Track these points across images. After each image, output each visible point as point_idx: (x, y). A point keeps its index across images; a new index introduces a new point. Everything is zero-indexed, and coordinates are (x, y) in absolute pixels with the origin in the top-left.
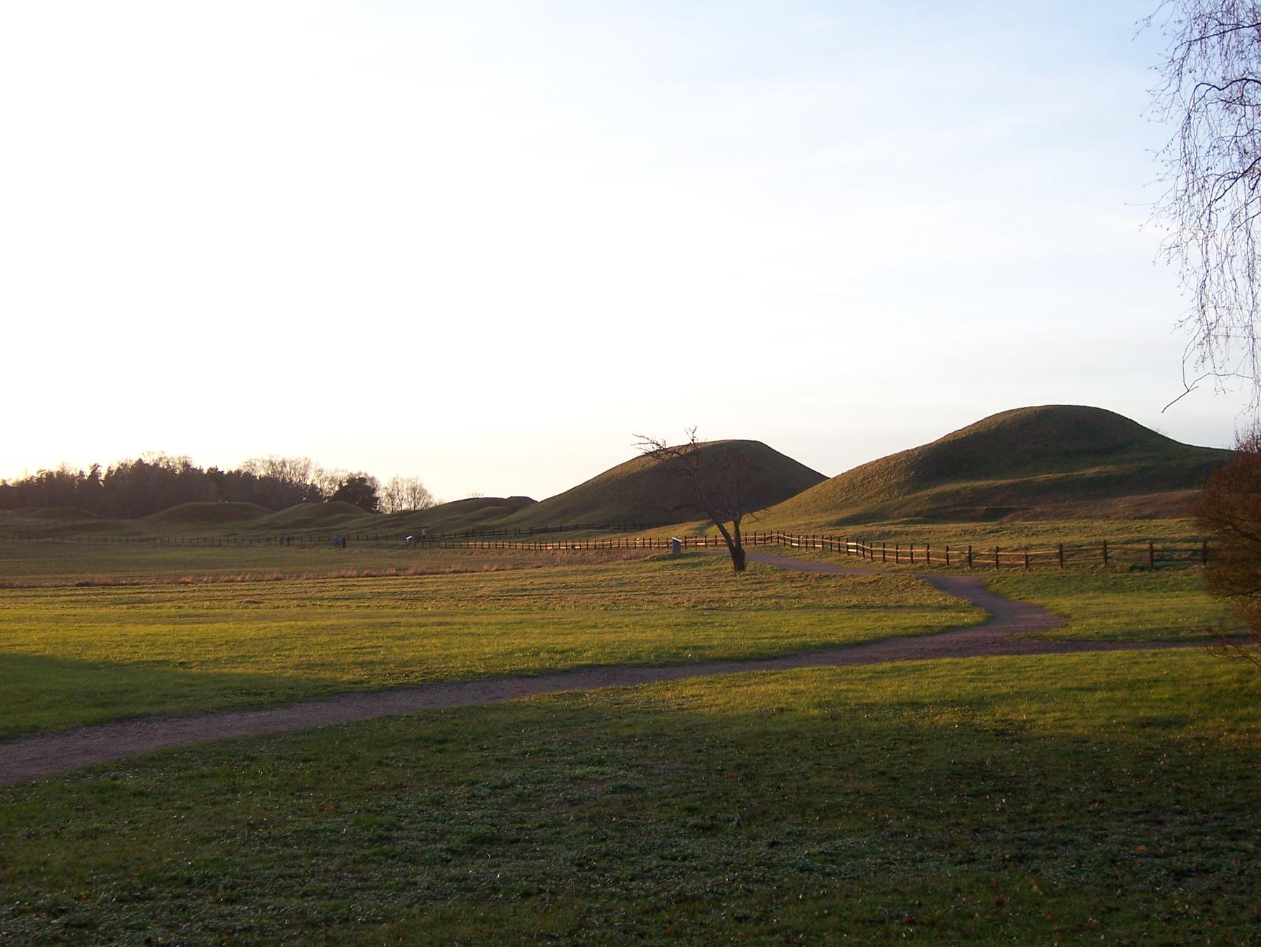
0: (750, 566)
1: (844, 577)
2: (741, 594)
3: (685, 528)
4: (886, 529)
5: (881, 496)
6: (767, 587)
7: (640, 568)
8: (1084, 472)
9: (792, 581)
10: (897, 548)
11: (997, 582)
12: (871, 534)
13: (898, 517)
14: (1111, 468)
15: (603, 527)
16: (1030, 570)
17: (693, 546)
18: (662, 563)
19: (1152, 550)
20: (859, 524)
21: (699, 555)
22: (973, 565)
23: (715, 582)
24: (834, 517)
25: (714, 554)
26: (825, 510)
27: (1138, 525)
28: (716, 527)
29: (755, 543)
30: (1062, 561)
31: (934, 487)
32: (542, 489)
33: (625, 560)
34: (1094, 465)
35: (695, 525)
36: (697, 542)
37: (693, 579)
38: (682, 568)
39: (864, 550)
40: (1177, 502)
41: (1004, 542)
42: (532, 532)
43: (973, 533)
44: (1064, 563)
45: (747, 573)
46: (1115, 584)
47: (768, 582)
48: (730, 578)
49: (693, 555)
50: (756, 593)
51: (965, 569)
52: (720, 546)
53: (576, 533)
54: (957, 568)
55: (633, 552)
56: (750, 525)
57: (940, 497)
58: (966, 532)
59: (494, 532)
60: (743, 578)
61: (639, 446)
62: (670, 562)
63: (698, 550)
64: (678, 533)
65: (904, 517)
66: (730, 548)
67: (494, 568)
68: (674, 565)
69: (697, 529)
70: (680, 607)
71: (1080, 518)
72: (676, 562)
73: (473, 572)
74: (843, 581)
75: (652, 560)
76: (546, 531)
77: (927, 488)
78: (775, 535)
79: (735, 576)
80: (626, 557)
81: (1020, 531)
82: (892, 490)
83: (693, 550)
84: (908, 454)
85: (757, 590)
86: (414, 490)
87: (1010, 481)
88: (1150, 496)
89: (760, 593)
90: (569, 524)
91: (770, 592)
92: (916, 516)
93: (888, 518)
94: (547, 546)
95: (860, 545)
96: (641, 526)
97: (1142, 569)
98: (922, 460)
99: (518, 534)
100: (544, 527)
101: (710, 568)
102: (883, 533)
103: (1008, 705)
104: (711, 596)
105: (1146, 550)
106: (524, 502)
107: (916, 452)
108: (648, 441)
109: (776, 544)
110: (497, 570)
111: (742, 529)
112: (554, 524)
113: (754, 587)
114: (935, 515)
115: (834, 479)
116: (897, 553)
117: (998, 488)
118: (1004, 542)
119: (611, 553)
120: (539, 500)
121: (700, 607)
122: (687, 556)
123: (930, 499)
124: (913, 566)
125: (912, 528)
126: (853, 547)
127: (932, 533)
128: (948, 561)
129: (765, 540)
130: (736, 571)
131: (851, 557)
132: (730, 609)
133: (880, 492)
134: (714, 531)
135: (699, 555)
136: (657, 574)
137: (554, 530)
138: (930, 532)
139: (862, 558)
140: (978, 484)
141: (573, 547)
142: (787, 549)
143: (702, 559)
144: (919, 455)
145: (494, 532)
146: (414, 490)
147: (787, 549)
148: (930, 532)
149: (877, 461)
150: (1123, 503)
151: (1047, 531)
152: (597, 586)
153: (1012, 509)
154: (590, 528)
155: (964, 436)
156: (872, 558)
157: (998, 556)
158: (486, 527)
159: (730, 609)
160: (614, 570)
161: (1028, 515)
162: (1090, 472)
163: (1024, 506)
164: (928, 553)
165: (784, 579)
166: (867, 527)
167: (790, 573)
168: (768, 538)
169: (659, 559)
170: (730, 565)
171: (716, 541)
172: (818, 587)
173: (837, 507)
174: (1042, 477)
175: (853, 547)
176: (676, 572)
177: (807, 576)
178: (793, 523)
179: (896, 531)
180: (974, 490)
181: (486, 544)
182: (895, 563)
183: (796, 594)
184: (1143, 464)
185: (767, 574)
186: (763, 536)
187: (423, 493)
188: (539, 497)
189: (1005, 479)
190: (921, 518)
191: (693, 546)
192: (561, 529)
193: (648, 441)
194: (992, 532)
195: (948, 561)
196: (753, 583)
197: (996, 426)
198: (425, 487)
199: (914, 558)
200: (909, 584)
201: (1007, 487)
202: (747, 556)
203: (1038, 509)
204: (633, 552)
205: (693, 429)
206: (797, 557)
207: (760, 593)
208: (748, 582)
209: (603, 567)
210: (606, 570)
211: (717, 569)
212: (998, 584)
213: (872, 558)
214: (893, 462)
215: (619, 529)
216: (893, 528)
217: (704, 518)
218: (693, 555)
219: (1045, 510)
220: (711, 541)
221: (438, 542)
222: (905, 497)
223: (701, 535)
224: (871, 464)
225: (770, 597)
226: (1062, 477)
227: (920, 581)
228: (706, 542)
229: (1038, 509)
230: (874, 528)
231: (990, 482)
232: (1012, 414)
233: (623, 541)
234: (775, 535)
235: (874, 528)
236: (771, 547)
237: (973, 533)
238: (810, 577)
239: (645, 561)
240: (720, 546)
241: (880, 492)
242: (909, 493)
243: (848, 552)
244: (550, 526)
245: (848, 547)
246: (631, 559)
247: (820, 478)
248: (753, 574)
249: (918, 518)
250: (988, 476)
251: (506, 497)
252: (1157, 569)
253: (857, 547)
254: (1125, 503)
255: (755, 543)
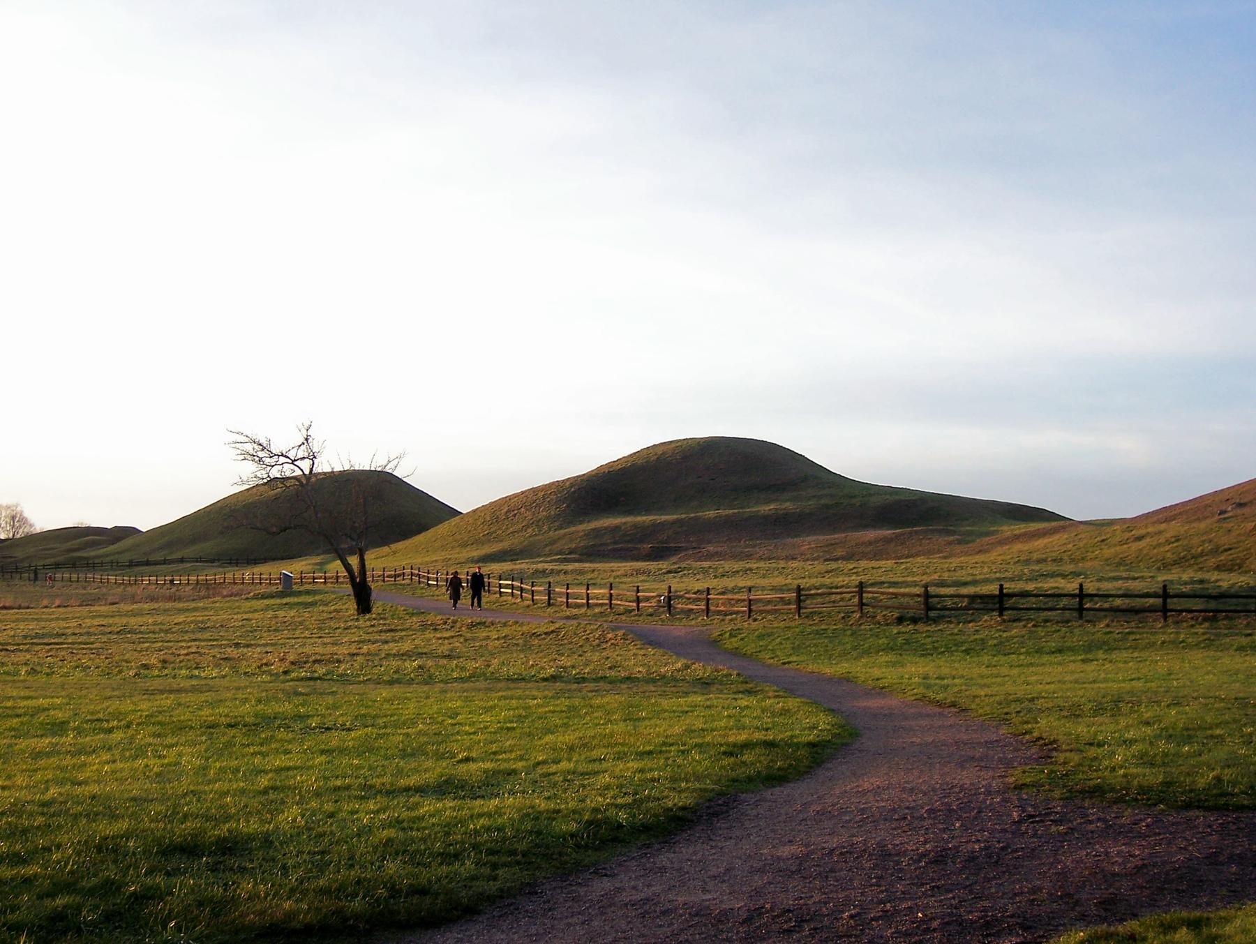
0: (377, 607)
1: (505, 624)
2: (365, 649)
3: (304, 563)
4: (540, 566)
5: (529, 530)
6: (401, 638)
7: (239, 607)
8: (759, 509)
9: (435, 630)
10: (567, 589)
11: (731, 636)
12: (521, 572)
13: (549, 555)
14: (788, 505)
15: (212, 561)
16: (755, 620)
17: (310, 583)
18: (267, 602)
19: (927, 596)
20: (505, 561)
21: (314, 592)
22: (673, 611)
23: (330, 627)
24: (477, 553)
25: (334, 592)
26: (464, 545)
27: (851, 567)
28: (339, 562)
29: (384, 581)
30: (799, 608)
31: (589, 522)
32: (146, 521)
33: (225, 597)
34: (768, 502)
35: (318, 559)
36: (314, 578)
37: (301, 623)
38: (291, 608)
39: (522, 590)
40: (870, 543)
41: (677, 584)
42: (132, 564)
43: (647, 573)
44: (801, 611)
45: (374, 616)
46: (907, 642)
47: (402, 630)
48: (350, 624)
49: (308, 592)
50: (386, 647)
51: (663, 616)
52: (342, 583)
53: (181, 566)
54: (651, 615)
55: (236, 588)
56: (378, 561)
57: (597, 533)
58: (638, 572)
59: (88, 564)
60: (368, 623)
61: (238, 445)
62: (278, 601)
63: (316, 587)
64: (290, 568)
65: (557, 554)
66: (353, 586)
67: (56, 605)
68: (282, 604)
69: (317, 564)
70: (264, 672)
71: (761, 559)
72: (285, 600)
73: (28, 608)
74: (506, 631)
75: (256, 597)
76: (148, 563)
77: (581, 522)
78: (408, 571)
79: (357, 620)
80: (225, 594)
81: (705, 571)
82: (541, 523)
83: (309, 587)
84: (558, 485)
85: (387, 642)
86: (13, 518)
87: (675, 517)
88: (836, 536)
89: (393, 647)
90: (174, 556)
91: (406, 646)
92: (570, 553)
93: (539, 556)
94: (142, 581)
95: (516, 584)
96: (255, 560)
97: (915, 621)
98: (575, 492)
99: (116, 566)
100: (145, 559)
101: (325, 609)
102: (537, 571)
103: (225, 515)
104: (320, 650)
105: (918, 596)
106: (131, 531)
107: (568, 483)
108: (247, 440)
109: (408, 581)
110: (59, 606)
111: (368, 565)
112: (158, 556)
113: (384, 636)
114: (593, 552)
115: (467, 513)
116: (533, 591)
117: (662, 524)
118: (677, 584)
119: (210, 589)
120: (144, 530)
121: (294, 675)
122: (300, 593)
123: (585, 535)
124: (589, 612)
125: (570, 567)
126: (507, 586)
127: (596, 573)
128: (638, 606)
129: (396, 576)
130: (359, 614)
131: (504, 598)
132: (344, 679)
133: (527, 526)
134: (336, 566)
135: (314, 592)
136: (256, 615)
137: (156, 563)
138: (593, 571)
139: (519, 600)
140: (639, 519)
141: (172, 581)
142: (422, 588)
143: (317, 598)
144: (572, 485)
145: (88, 564)
146: (13, 518)
147: (422, 588)
148: (593, 571)
149: (523, 493)
150: (809, 542)
151: (738, 572)
152: (167, 631)
153: (680, 547)
154: (197, 562)
155: (620, 467)
156: (533, 600)
157: (708, 599)
158: (81, 558)
159: (344, 679)
160: (205, 609)
161: (700, 554)
162: (766, 509)
163: (694, 545)
164: (611, 595)
165: (424, 627)
166: (515, 564)
167: (431, 618)
168: (399, 575)
169: (264, 597)
170: (352, 606)
171: (338, 577)
172: (474, 639)
173: (478, 542)
174: (711, 514)
175: (507, 586)
176: (281, 613)
177: (455, 622)
178: (427, 559)
179: (552, 570)
180: (635, 526)
181: (74, 576)
182: (564, 607)
183: (445, 649)
184: (823, 502)
185: (400, 619)
186: (393, 573)
187: (23, 521)
188: (144, 528)
189: (669, 514)
190: (577, 556)
191: (310, 583)
192: (165, 562)
193: (247, 440)
194: (670, 572)
195: (638, 606)
196: (381, 631)
197: (656, 457)
198: (26, 514)
199: (613, 602)
200: (604, 637)
201: (674, 523)
202: (374, 596)
203: (711, 548)
204: (236, 588)
205: (307, 425)
206: (436, 598)
207: (393, 647)
208: (375, 629)
209: (193, 605)
210: (195, 609)
211: (335, 611)
212: (734, 640)
213: (533, 600)
214: (541, 494)
215: (230, 563)
216: (546, 566)
217: (325, 552)
218: (308, 592)
219: (719, 549)
220: (332, 578)
221: (21, 573)
222: (557, 532)
223: (320, 570)
224: (515, 496)
225: (407, 655)
226: (734, 513)
227: (620, 633)
228: (325, 578)
229: (711, 548)
230: (521, 565)
231: (651, 518)
232: (673, 445)
233: (229, 575)
234: (408, 571)
235: (523, 566)
236: (403, 585)
237: (647, 573)
238: (458, 625)
239: (247, 599)
240: (342, 583)
241: (527, 526)
242: (561, 528)
243: (501, 592)
244: (151, 558)
245: (500, 586)
246: (231, 596)
247: (455, 513)
248: (381, 619)
249: (573, 556)
250: (648, 511)
251: (109, 525)
252: (935, 621)
253: (512, 587)
254: (809, 544)
255: (384, 581)
